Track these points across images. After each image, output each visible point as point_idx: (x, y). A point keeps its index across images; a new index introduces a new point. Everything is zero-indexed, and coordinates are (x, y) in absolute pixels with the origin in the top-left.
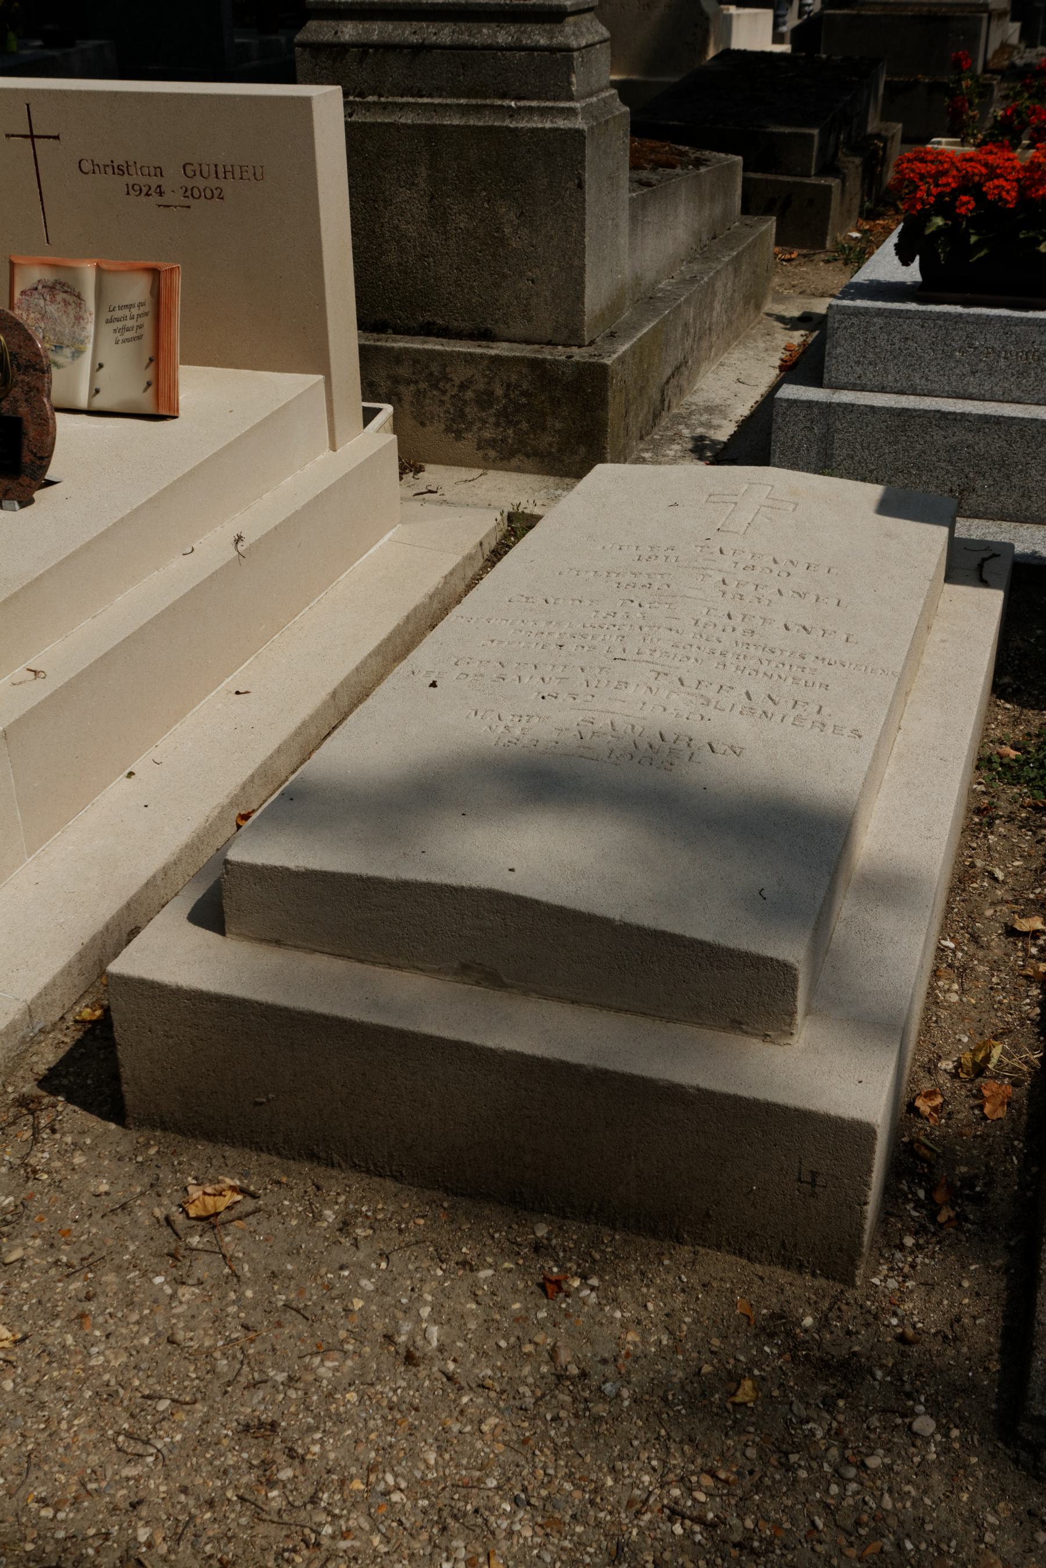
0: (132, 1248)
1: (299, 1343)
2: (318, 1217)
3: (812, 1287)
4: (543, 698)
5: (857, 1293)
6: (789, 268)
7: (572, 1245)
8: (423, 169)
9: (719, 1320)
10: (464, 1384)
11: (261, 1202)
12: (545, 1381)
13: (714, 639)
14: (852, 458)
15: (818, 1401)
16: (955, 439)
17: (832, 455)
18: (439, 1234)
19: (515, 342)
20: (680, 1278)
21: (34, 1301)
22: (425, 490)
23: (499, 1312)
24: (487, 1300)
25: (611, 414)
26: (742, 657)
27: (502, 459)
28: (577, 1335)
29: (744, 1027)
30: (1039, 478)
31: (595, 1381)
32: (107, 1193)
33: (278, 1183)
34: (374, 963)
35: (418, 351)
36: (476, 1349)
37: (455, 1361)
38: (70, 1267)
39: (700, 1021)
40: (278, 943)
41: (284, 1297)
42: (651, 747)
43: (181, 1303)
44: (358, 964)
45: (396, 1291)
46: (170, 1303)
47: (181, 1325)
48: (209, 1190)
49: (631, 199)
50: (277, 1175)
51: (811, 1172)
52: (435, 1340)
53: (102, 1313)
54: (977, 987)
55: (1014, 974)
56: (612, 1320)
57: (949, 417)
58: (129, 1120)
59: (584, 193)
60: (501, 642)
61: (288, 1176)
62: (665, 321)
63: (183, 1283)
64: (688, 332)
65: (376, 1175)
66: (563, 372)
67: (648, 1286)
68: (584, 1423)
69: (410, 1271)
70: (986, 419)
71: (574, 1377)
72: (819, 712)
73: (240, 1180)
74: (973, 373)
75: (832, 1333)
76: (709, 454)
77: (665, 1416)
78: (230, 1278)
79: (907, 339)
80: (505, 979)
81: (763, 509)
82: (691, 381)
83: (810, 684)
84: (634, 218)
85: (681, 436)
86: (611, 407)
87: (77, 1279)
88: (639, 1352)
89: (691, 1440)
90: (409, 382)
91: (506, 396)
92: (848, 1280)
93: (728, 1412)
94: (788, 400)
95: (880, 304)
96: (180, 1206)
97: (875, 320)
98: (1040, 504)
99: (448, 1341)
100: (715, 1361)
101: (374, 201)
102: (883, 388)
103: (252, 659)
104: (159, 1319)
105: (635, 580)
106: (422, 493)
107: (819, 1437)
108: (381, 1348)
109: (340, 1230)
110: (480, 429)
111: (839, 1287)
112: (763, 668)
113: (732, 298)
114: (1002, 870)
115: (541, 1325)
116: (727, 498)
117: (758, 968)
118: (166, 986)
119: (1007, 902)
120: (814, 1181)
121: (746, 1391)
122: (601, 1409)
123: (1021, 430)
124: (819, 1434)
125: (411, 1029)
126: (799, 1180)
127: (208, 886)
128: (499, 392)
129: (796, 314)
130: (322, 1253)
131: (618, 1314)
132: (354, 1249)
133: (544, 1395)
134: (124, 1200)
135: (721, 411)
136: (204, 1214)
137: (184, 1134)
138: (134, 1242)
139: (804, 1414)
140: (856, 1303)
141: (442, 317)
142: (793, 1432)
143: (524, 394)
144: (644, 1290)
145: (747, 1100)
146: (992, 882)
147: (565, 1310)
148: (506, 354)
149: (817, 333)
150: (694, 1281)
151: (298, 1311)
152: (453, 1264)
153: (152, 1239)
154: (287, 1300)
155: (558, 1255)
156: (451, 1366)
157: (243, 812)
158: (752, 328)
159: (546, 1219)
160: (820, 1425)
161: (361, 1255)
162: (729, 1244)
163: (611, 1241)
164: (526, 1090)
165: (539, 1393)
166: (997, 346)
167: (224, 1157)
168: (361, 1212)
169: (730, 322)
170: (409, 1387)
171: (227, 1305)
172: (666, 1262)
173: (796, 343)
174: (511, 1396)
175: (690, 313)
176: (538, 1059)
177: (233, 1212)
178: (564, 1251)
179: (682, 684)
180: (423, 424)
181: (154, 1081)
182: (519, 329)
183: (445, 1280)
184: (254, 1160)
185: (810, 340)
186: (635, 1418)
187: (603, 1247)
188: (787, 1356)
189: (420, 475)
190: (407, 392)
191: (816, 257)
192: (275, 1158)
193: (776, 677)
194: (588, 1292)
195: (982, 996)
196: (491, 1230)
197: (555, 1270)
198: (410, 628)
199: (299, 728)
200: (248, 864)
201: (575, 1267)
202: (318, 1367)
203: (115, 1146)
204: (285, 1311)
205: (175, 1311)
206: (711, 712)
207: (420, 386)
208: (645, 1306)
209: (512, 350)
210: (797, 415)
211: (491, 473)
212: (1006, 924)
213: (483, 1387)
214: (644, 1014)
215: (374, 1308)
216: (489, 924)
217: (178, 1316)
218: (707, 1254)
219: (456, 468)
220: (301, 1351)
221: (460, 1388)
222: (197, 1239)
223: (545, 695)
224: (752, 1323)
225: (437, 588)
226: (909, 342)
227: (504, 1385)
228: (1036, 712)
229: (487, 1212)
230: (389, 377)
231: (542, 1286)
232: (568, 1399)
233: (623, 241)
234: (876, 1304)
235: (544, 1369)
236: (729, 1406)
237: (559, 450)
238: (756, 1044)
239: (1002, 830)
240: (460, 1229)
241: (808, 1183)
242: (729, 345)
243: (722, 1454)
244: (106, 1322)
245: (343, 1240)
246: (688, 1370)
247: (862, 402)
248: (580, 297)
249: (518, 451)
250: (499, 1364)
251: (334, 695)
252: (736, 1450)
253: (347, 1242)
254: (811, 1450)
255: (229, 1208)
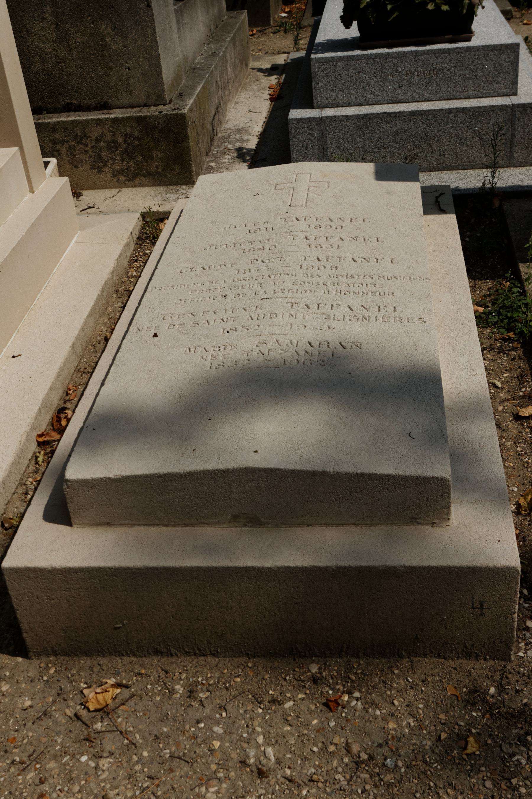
0: (59, 741)
1: (188, 780)
2: (172, 692)
3: (486, 667)
4: (228, 332)
5: (513, 664)
6: (254, 40)
7: (336, 674)
8: (48, 8)
9: (440, 702)
10: (300, 782)
11: (133, 690)
12: (348, 767)
13: (315, 275)
14: (339, 148)
15: (516, 741)
16: (397, 128)
17: (327, 148)
18: (252, 685)
19: (124, 108)
20: (407, 680)
21: (6, 793)
22: (86, 207)
23: (305, 728)
24: (295, 722)
25: (191, 144)
26: (336, 284)
27: (129, 181)
28: (358, 732)
29: (419, 520)
30: (448, 143)
31: (379, 759)
32: (31, 707)
33: (140, 674)
34: (174, 526)
35: (66, 122)
36: (299, 756)
37: (289, 768)
38: (23, 764)
39: (390, 522)
40: (109, 524)
41: (168, 751)
42: (306, 352)
43: (103, 771)
44: (164, 528)
45: (238, 730)
46: (96, 773)
47: (108, 786)
48: (99, 690)
49: (175, 10)
50: (137, 669)
51: (480, 601)
52: (273, 756)
53: (54, 790)
54: (510, 455)
55: (528, 443)
56: (376, 718)
57: (392, 115)
58: (31, 654)
59: (152, 10)
60: (186, 300)
61: (145, 669)
62: (207, 82)
63: (101, 757)
64: (218, 86)
65: (201, 656)
66: (158, 122)
67: (390, 690)
68: (382, 790)
69: (241, 714)
70: (413, 113)
71: (366, 761)
72: (395, 311)
73: (115, 678)
74: (400, 87)
75: (508, 694)
76: (248, 158)
77: (429, 773)
78: (130, 746)
79: (359, 72)
80: (262, 520)
81: (310, 188)
82: (224, 116)
83: (382, 294)
84: (178, 21)
85: (228, 150)
86: (190, 139)
87: (30, 771)
88: (399, 734)
89: (450, 784)
90: (63, 142)
91: (125, 142)
92: (507, 658)
93: (465, 760)
94: (296, 119)
95: (339, 54)
96: (81, 704)
97: (339, 64)
98: (451, 158)
99: (281, 755)
100: (447, 729)
101: (20, 32)
102: (349, 104)
103: (15, 333)
104: (93, 785)
105: (253, 246)
106: (85, 209)
107: (524, 764)
108: (241, 770)
109: (189, 697)
110: (112, 164)
111: (502, 663)
112: (352, 289)
113: (235, 62)
114: (499, 381)
115: (334, 731)
116: (287, 185)
117: (425, 485)
118: (45, 569)
119: (508, 400)
120: (482, 606)
121: (472, 747)
122: (389, 778)
123: (434, 117)
124: (524, 762)
125: (214, 565)
126: (473, 608)
127: (49, 494)
128: (121, 140)
129: (268, 66)
130: (182, 715)
131: (378, 712)
132: (202, 707)
133: (351, 777)
134: (43, 709)
135: (246, 131)
136: (98, 707)
137: (69, 656)
138: (59, 736)
139: (510, 751)
140: (514, 671)
141: (76, 99)
142: (508, 764)
143: (136, 139)
144: (388, 692)
145: (436, 568)
146: (496, 389)
147: (345, 717)
148: (121, 116)
149: (284, 76)
150: (416, 680)
151: (180, 758)
152: (267, 703)
153: (70, 731)
154: (171, 753)
155: (329, 682)
156: (288, 772)
157: (39, 433)
158: (247, 78)
159: (314, 660)
160: (522, 756)
161: (208, 711)
162: (432, 652)
163: (358, 666)
164: (293, 588)
165: (348, 777)
166: (412, 69)
167: (99, 665)
168: (198, 682)
169: (236, 76)
170: (267, 793)
171: (134, 765)
172: (396, 672)
173: (274, 84)
174: (332, 783)
175: (217, 74)
176: (300, 568)
177: (117, 700)
178: (332, 678)
179: (309, 308)
180: (76, 167)
181: (44, 627)
182: (125, 99)
183: (265, 715)
184: (120, 662)
185: (282, 80)
186: (411, 778)
187: (355, 671)
188: (488, 716)
189: (81, 198)
190: (63, 148)
191: (267, 31)
192: (133, 659)
193: (361, 293)
194: (355, 702)
195: (515, 460)
196: (283, 675)
197: (331, 692)
198: (105, 295)
199: (59, 372)
200: (82, 479)
201: (342, 688)
202: (206, 794)
203: (25, 673)
204: (172, 760)
205: (101, 777)
206: (333, 323)
207: (71, 144)
208: (393, 703)
209: (123, 113)
210: (303, 128)
211: (124, 190)
212: (512, 413)
213: (313, 781)
214: (355, 524)
215: (227, 744)
216: (248, 488)
217: (104, 781)
218: (419, 661)
219: (102, 190)
220: (191, 785)
221: (299, 785)
222: (100, 724)
223: (229, 330)
224: (460, 699)
225: (114, 267)
226: (361, 74)
227: (325, 776)
228: (483, 281)
229: (277, 664)
230: (50, 141)
231: (326, 705)
232: (367, 776)
233: (175, 36)
234: (526, 669)
235: (346, 760)
236: (465, 757)
237: (163, 170)
238: (428, 529)
239: (489, 356)
240: (263, 678)
241: (478, 608)
242: (237, 90)
243: (472, 789)
244: (59, 796)
245: (193, 704)
246: (432, 739)
247: (339, 114)
248: (159, 75)
249: (138, 174)
250: (317, 763)
251: (73, 347)
252: (479, 785)
253: (196, 704)
254: (523, 773)
255: (114, 699)
